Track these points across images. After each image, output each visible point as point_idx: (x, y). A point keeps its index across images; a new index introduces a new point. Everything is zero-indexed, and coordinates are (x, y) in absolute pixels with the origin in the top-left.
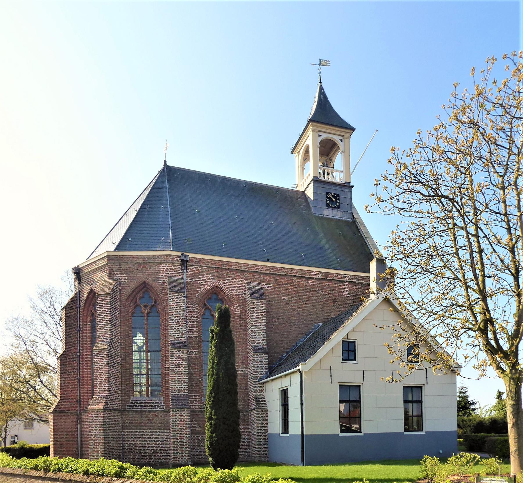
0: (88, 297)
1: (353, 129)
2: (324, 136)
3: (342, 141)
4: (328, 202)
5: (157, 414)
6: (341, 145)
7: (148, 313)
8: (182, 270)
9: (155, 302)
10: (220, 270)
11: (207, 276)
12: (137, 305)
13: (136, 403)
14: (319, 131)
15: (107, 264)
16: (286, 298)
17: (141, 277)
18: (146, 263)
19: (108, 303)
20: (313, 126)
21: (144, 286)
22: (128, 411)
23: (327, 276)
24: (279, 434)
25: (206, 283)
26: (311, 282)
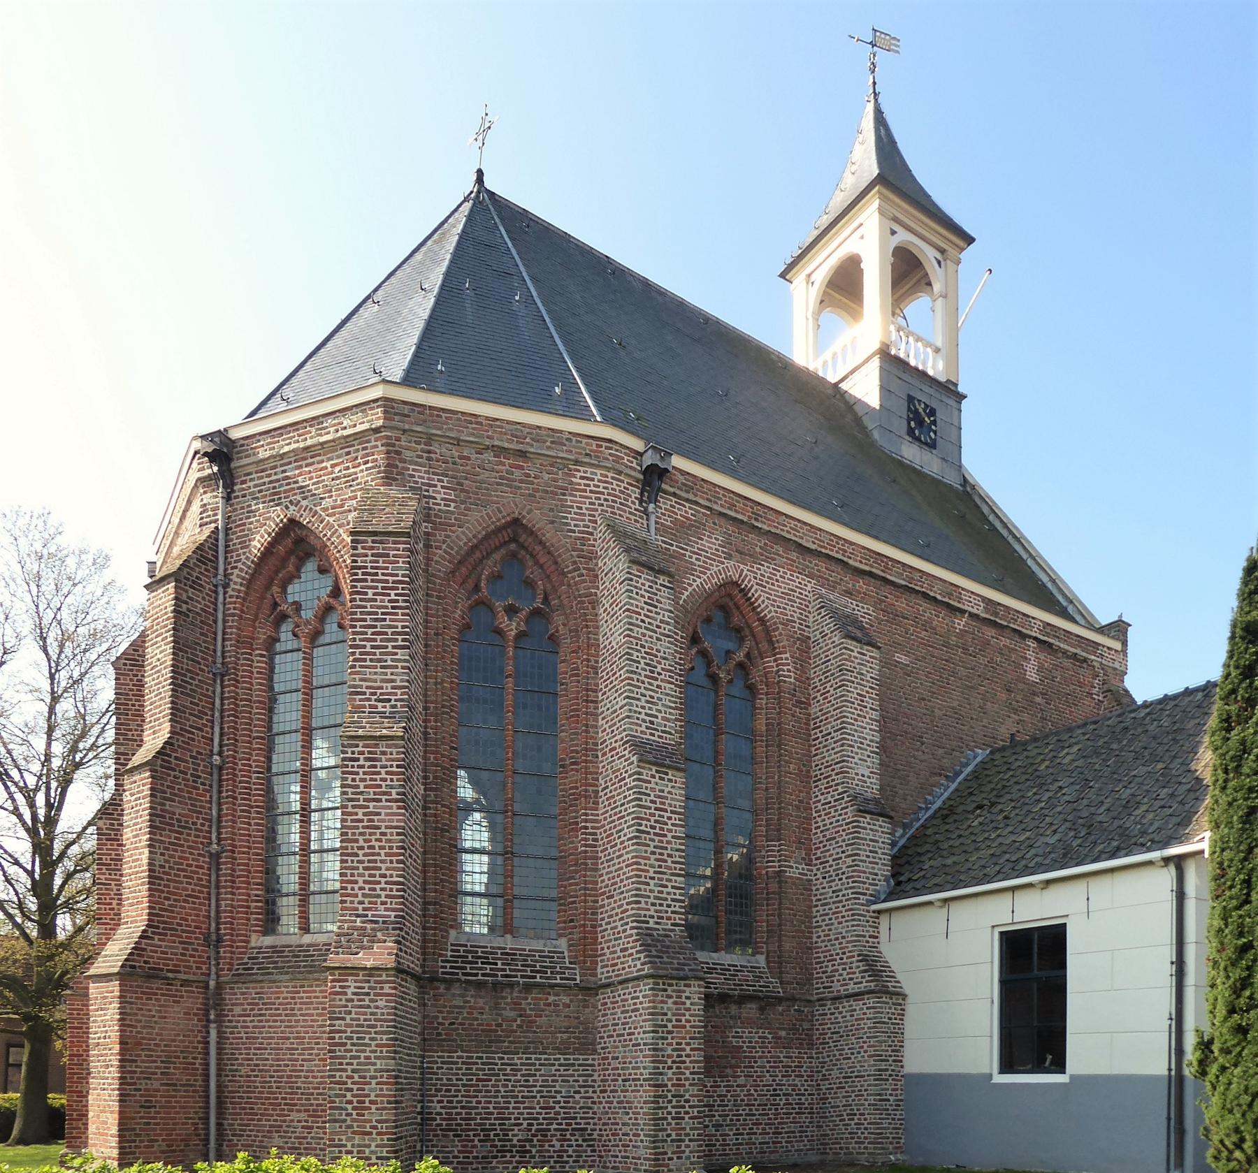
0: (268, 551)
1: (970, 240)
2: (903, 236)
3: (939, 263)
5: (551, 998)
7: (521, 635)
8: (641, 501)
9: (546, 600)
10: (746, 527)
11: (711, 542)
12: (481, 603)
13: (472, 954)
14: (895, 220)
15: (376, 430)
16: (903, 659)
17: (508, 503)
18: (522, 454)
19: (400, 569)
20: (882, 197)
21: (514, 539)
22: (449, 983)
24: (991, 1076)
25: (709, 562)
26: (960, 623)
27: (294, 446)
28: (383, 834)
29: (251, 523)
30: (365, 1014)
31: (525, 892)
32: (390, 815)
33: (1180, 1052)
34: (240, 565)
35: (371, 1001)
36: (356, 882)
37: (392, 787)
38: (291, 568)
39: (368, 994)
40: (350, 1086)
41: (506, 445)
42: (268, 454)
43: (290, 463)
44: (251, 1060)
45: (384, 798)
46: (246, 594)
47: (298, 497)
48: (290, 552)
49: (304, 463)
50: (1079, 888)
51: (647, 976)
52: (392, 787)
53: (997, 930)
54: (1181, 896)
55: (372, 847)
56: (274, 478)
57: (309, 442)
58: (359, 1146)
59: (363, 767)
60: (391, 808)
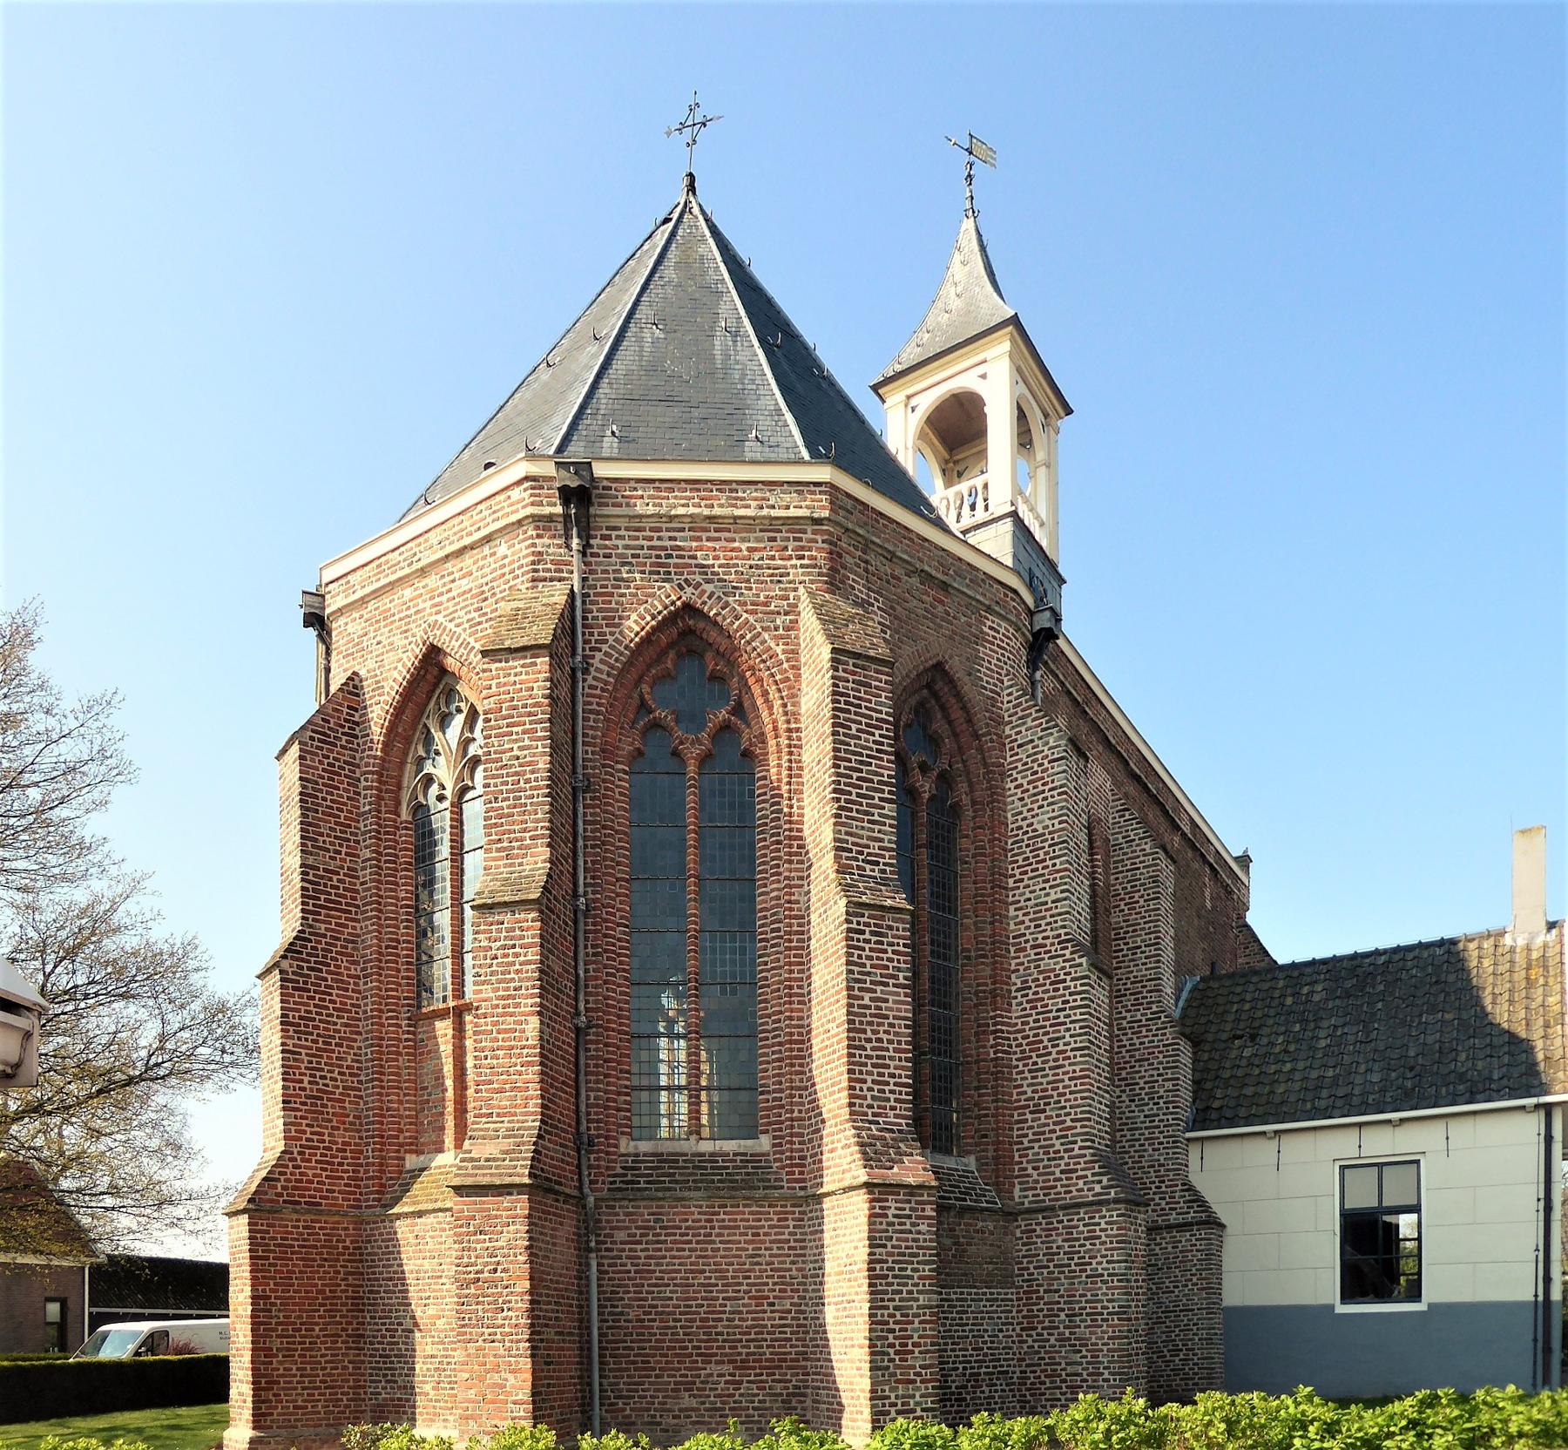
1: (1069, 411)
15: (817, 521)
18: (945, 587)
20: (1013, 341)
27: (692, 510)
28: (892, 1025)
29: (623, 595)
30: (907, 1240)
32: (898, 1004)
33: (1548, 1280)
34: (605, 648)
35: (913, 1225)
36: (865, 1081)
37: (899, 970)
39: (909, 1217)
40: (892, 1326)
41: (934, 573)
42: (651, 510)
43: (683, 530)
44: (646, 1299)
45: (891, 981)
46: (615, 689)
47: (698, 578)
48: (671, 645)
49: (704, 535)
50: (1438, 1129)
51: (1116, 1201)
52: (899, 970)
53: (1338, 1164)
54: (1549, 1139)
55: (880, 1040)
56: (656, 543)
57: (717, 511)
58: (904, 1397)
59: (868, 941)
60: (898, 994)
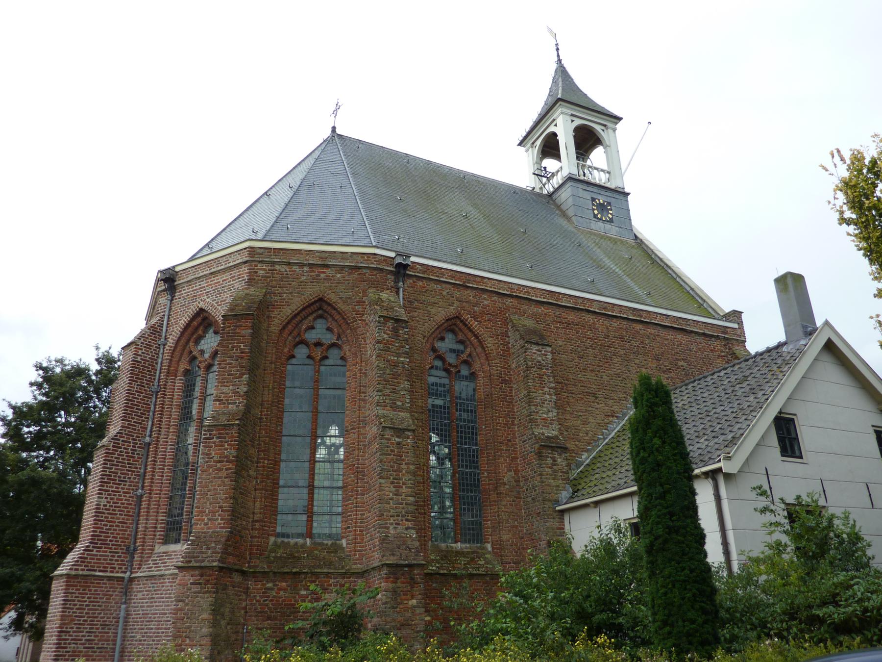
1: (620, 119)
2: (578, 122)
4: (596, 212)
6: (605, 135)
14: (572, 115)
15: (245, 263)
23: (641, 316)
31: (321, 510)
38: (200, 332)
